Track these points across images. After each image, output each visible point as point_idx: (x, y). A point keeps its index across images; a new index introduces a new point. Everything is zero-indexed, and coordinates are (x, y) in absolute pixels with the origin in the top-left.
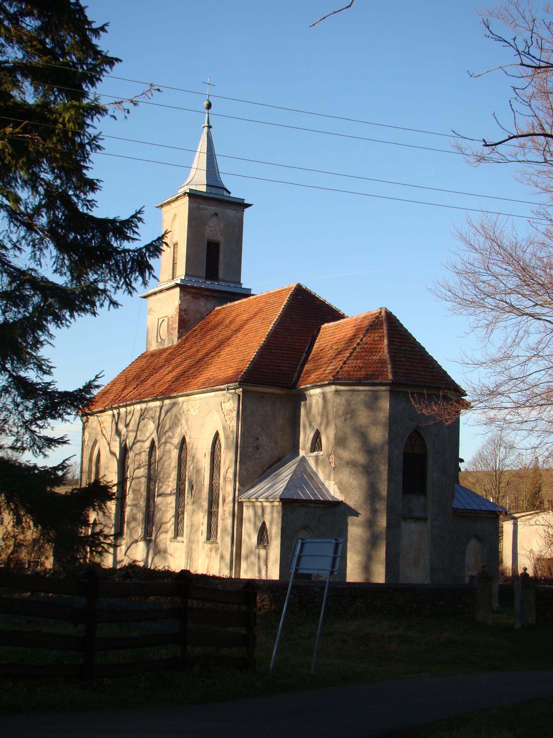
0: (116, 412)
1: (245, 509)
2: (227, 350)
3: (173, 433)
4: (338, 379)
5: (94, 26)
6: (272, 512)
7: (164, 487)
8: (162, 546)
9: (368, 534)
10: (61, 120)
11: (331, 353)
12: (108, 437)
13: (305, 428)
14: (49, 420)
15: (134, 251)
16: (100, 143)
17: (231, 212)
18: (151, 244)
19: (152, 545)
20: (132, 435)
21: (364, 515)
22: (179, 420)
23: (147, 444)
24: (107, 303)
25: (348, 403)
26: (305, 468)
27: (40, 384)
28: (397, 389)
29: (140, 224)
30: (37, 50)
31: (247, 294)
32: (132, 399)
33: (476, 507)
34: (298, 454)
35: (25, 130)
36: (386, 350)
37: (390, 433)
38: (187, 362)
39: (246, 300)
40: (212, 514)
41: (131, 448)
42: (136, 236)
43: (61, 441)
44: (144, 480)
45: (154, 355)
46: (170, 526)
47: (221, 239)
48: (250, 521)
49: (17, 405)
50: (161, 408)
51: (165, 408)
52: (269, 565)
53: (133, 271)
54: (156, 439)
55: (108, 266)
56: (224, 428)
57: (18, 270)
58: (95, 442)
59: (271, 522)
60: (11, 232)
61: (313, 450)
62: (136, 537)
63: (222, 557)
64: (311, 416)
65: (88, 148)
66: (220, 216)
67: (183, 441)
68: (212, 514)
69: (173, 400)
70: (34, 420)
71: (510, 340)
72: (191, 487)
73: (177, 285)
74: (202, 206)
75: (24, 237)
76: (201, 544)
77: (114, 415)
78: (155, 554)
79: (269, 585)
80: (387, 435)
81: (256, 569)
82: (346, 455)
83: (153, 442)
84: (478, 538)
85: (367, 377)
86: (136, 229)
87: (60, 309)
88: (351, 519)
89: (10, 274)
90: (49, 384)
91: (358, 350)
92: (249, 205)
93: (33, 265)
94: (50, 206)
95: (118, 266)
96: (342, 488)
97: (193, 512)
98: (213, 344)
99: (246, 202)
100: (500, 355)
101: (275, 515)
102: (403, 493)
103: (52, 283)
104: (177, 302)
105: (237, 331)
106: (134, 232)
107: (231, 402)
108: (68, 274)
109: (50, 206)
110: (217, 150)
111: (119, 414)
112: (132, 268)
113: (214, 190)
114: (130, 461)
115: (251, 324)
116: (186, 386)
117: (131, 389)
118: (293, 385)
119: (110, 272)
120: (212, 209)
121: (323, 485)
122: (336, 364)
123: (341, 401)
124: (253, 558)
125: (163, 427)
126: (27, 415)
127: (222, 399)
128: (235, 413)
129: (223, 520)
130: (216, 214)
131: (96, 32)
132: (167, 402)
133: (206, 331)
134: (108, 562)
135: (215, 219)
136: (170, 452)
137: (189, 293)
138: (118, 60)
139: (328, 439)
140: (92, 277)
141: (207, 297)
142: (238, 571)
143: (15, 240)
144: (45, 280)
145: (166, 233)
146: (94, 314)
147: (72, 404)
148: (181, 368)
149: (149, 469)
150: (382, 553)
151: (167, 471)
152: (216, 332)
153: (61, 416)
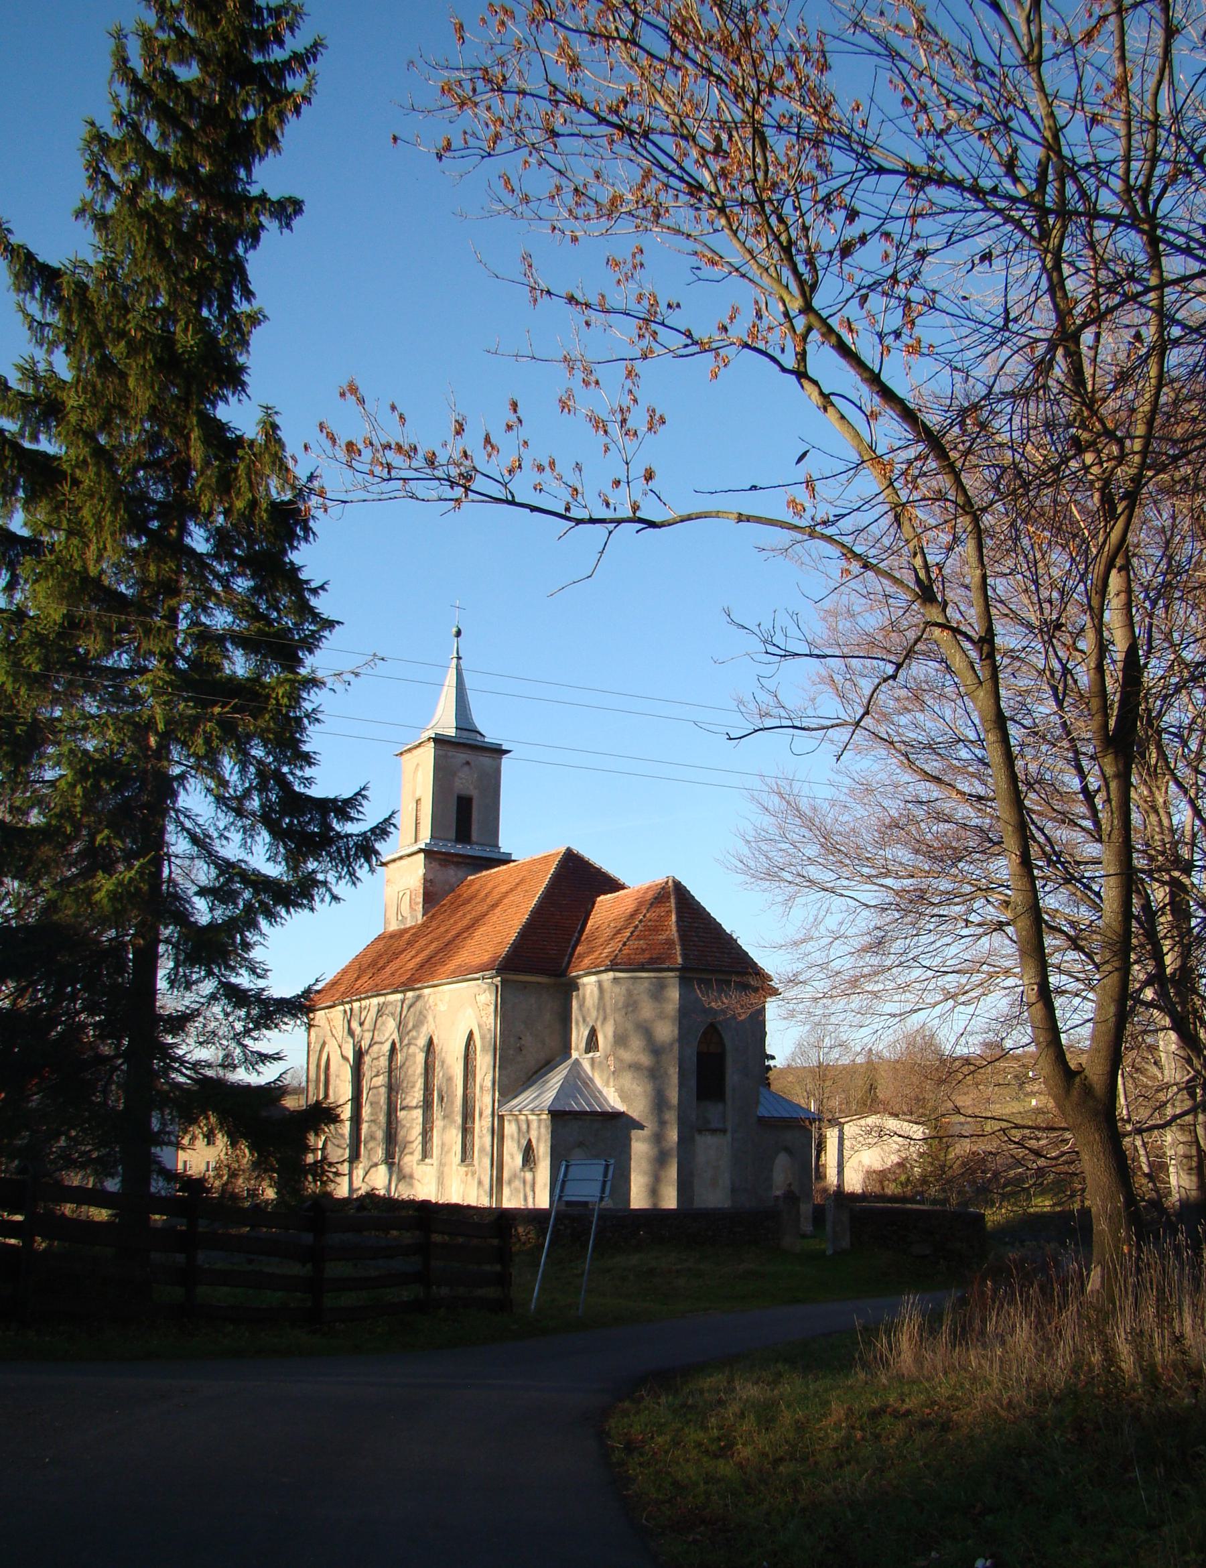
0: (347, 1007)
1: (506, 1123)
2: (482, 930)
3: (418, 1032)
4: (617, 964)
5: (313, 585)
6: (539, 1127)
7: (409, 1099)
8: (407, 1170)
9: (656, 1150)
10: (274, 695)
11: (608, 932)
12: (340, 1039)
13: (577, 1024)
14: (265, 1031)
15: (358, 835)
16: (319, 716)
17: (485, 760)
18: (377, 827)
19: (395, 1169)
20: (368, 1035)
21: (650, 1127)
22: (425, 1017)
23: (387, 1046)
24: (328, 898)
25: (629, 993)
26: (579, 1073)
27: (251, 990)
28: (688, 975)
29: (364, 802)
30: (248, 616)
31: (506, 860)
32: (366, 992)
33: (786, 1115)
34: (570, 1056)
35: (235, 709)
36: (674, 928)
37: (680, 1029)
38: (434, 945)
39: (504, 867)
40: (466, 1130)
41: (367, 1052)
42: (361, 816)
43: (277, 1057)
44: (383, 1090)
45: (394, 936)
46: (417, 1146)
47: (475, 793)
48: (512, 1138)
49: (227, 1015)
50: (403, 1002)
51: (407, 1003)
52: (537, 1191)
53: (357, 857)
54: (397, 1041)
55: (329, 854)
56: (480, 1026)
57: (224, 860)
58: (324, 1044)
59: (538, 1140)
60: (218, 819)
61: (588, 1050)
62: (375, 1160)
63: (480, 1183)
64: (585, 1009)
65: (306, 721)
66: (472, 764)
67: (430, 1042)
68: (466, 1130)
69: (417, 992)
70: (247, 1032)
71: (811, 919)
72: (441, 1099)
73: (421, 850)
74: (450, 754)
75: (232, 823)
76: (454, 1167)
77: (345, 1011)
78: (399, 1180)
79: (535, 1217)
80: (676, 1032)
81: (522, 1196)
82: (627, 1056)
83: (393, 1044)
84: (788, 1150)
85: (652, 961)
86: (360, 808)
87: (275, 905)
88: (635, 1134)
89: (217, 866)
90: (263, 990)
91: (640, 928)
92: (508, 752)
93: (242, 855)
94: (262, 788)
95: (340, 853)
96: (623, 1097)
97: (444, 1128)
98: (465, 922)
99: (504, 748)
100: (800, 936)
101: (543, 1130)
102: (698, 1099)
103: (264, 875)
104: (421, 871)
105: (494, 906)
106: (359, 812)
107: (487, 993)
108: (283, 863)
109: (262, 788)
110: (468, 683)
111: (351, 1010)
112: (356, 854)
113: (465, 734)
114: (365, 1067)
115: (511, 897)
116: (432, 975)
117: (366, 978)
118: (563, 973)
119: (331, 861)
120: (462, 756)
121: (600, 1092)
122: (615, 945)
123: (620, 991)
124: (517, 1183)
125: (406, 1026)
126: (239, 1026)
127: (476, 990)
128: (492, 1008)
129: (480, 1137)
130: (468, 763)
131: (315, 592)
132: (410, 994)
133: (457, 905)
134: (341, 1190)
135: (466, 768)
136: (414, 1055)
137: (435, 860)
138: (338, 622)
139: (605, 1037)
140: (312, 865)
141: (457, 864)
142: (499, 1199)
143: (222, 827)
144: (256, 873)
145: (394, 813)
146: (312, 909)
147: (289, 1012)
148: (427, 952)
149: (390, 1077)
150: (672, 1172)
151: (411, 1079)
152: (469, 907)
153: (277, 1026)
